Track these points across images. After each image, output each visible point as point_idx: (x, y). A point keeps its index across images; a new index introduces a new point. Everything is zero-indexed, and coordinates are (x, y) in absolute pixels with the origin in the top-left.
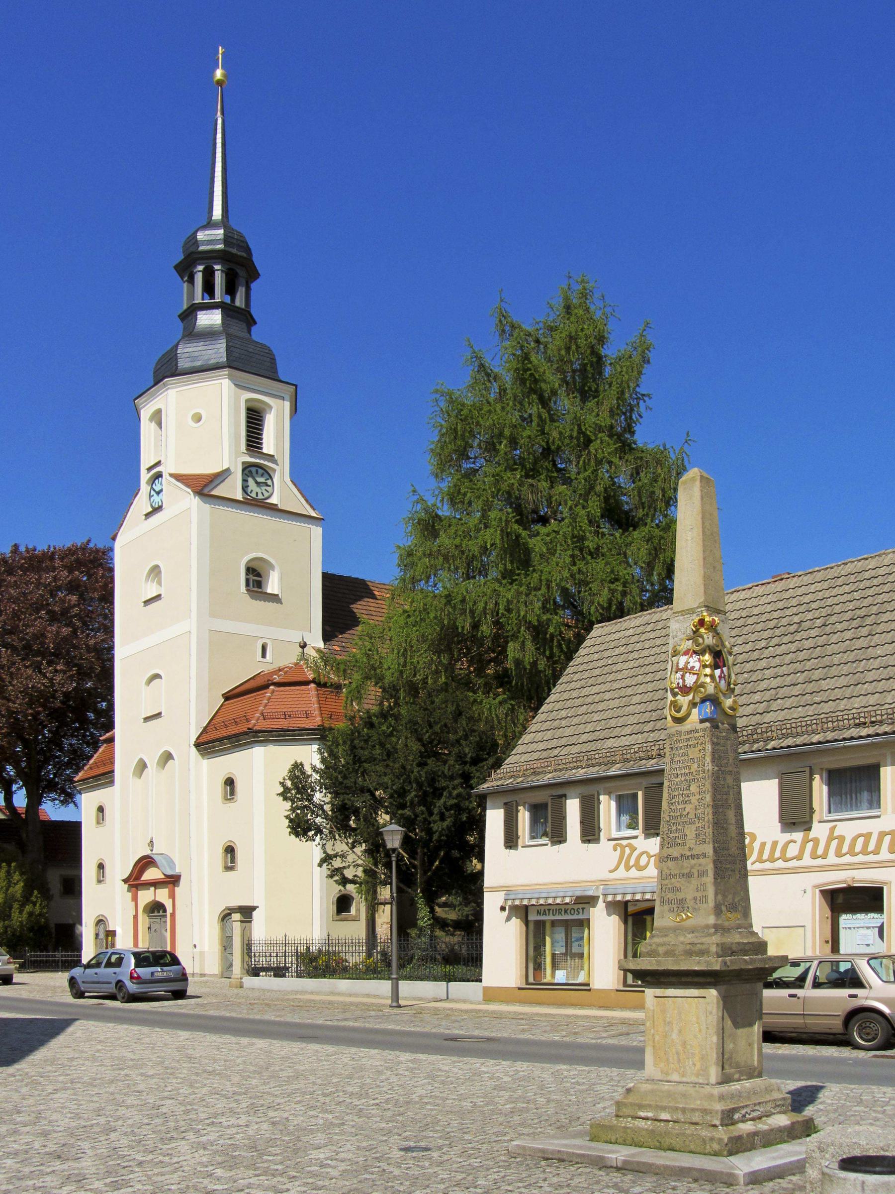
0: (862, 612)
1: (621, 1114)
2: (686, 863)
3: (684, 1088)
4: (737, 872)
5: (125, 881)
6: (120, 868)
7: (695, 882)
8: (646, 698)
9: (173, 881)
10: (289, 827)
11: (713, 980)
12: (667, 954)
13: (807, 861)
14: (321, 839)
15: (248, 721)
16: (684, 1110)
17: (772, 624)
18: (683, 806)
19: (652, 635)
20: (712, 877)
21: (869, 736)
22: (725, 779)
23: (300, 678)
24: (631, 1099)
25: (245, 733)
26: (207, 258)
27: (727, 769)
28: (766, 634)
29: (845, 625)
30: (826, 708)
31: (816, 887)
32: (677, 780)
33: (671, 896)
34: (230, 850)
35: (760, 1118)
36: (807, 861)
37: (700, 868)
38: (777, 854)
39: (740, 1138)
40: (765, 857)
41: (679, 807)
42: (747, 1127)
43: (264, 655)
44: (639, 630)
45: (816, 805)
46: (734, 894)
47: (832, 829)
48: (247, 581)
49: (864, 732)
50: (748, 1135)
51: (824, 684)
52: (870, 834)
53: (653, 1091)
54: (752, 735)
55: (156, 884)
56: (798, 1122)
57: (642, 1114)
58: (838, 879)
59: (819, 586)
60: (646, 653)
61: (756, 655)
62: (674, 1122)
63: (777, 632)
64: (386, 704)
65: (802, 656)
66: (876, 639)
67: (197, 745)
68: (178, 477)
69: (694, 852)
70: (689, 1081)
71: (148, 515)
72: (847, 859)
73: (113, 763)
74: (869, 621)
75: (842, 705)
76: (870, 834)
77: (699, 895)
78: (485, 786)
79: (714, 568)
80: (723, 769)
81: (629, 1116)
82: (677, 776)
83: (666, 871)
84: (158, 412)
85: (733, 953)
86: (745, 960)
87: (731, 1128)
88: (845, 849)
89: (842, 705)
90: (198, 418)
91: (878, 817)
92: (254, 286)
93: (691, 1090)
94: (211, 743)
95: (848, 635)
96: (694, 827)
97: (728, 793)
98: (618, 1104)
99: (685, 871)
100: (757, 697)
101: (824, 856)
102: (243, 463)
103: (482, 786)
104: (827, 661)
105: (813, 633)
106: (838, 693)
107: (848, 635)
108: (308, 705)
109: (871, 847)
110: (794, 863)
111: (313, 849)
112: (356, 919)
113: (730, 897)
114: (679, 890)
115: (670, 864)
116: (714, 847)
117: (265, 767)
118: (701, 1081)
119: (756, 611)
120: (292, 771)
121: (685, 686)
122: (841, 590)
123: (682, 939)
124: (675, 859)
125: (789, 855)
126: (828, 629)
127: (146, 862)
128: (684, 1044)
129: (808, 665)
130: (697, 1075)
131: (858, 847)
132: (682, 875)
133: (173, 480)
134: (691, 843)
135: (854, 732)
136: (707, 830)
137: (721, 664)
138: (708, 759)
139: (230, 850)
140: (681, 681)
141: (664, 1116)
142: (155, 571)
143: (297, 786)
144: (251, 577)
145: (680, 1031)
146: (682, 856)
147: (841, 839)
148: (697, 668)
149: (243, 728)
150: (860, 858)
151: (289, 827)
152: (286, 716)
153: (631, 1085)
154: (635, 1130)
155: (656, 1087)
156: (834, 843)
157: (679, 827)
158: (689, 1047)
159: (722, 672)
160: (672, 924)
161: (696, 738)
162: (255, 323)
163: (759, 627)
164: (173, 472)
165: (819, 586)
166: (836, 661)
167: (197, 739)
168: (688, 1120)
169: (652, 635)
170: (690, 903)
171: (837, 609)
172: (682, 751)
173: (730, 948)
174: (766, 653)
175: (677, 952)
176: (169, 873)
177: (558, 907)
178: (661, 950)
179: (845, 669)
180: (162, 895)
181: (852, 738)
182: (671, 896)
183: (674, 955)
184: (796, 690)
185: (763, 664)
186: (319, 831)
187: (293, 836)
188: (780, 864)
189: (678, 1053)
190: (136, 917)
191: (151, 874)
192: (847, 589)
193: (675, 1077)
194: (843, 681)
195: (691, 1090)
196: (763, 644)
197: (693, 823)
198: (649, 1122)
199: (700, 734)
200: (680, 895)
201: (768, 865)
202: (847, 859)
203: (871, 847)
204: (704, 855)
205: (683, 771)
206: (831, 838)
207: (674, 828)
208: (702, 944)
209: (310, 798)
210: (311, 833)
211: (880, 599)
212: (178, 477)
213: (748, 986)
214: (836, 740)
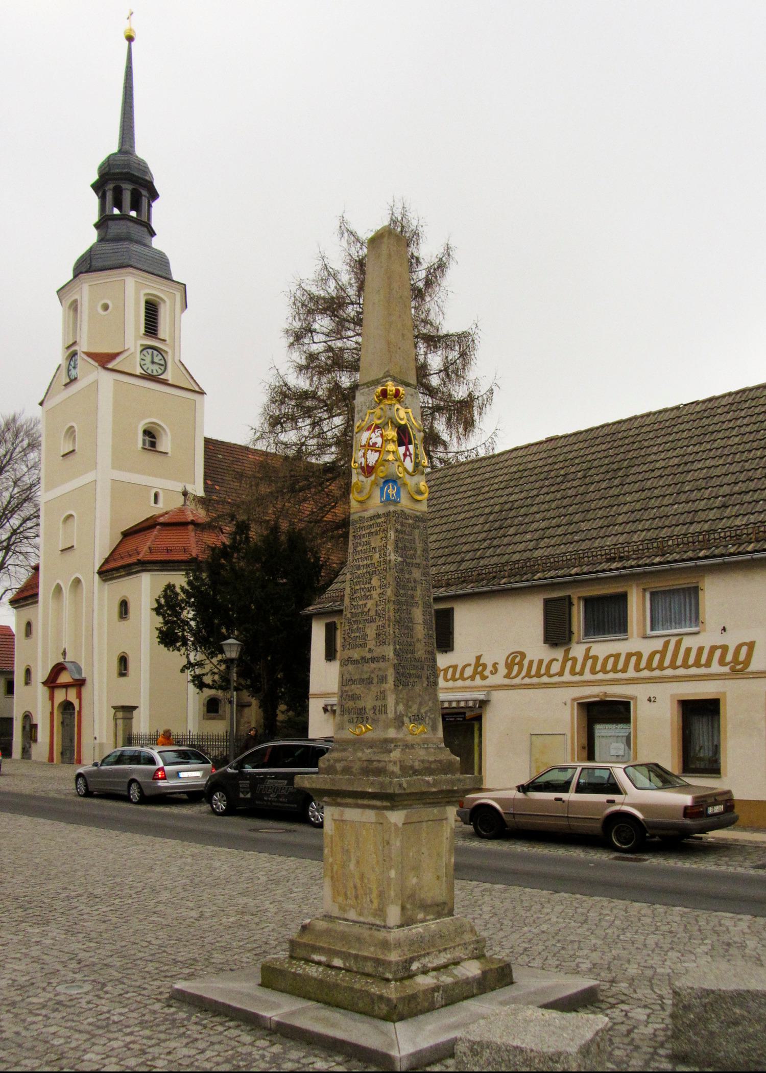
0: (615, 466)
1: (295, 955)
3: (360, 930)
4: (424, 679)
5: (44, 683)
6: (41, 674)
7: (374, 689)
8: (441, 536)
9: (80, 684)
10: (158, 637)
11: (388, 804)
12: (347, 770)
13: (567, 677)
14: (187, 649)
15: (138, 553)
16: (356, 957)
17: (542, 476)
18: (364, 602)
19: (448, 486)
20: (393, 683)
21: (617, 569)
22: (410, 573)
23: (183, 520)
24: (305, 940)
25: (134, 564)
26: (116, 179)
27: (415, 561)
28: (537, 485)
29: (601, 477)
30: (584, 546)
31: (574, 700)
32: (359, 572)
33: (350, 704)
34: (123, 661)
35: (445, 966)
36: (567, 677)
37: (381, 673)
38: (543, 671)
39: (414, 997)
40: (533, 672)
41: (360, 603)
42: (425, 981)
43: (156, 502)
44: (438, 482)
45: (575, 628)
48: (144, 441)
49: (614, 566)
50: (425, 992)
51: (583, 526)
53: (328, 932)
54: (523, 568)
55: (66, 686)
56: (491, 970)
57: (316, 957)
58: (592, 693)
59: (581, 445)
60: (442, 500)
61: (529, 501)
62: (347, 970)
63: (547, 483)
64: (238, 537)
65: (565, 502)
66: (626, 488)
67: (100, 573)
68: (89, 355)
69: (375, 655)
70: (366, 921)
71: (66, 385)
72: (600, 676)
73: (38, 587)
74: (620, 473)
75: (597, 543)
77: (378, 703)
79: (403, 335)
80: (408, 560)
81: (301, 959)
82: (358, 568)
83: (347, 676)
84: (76, 301)
85: (416, 772)
86: (428, 782)
87: (407, 982)
88: (598, 668)
89: (597, 543)
90: (106, 307)
91: (626, 639)
92: (155, 205)
93: (366, 933)
94: (107, 572)
95: (604, 485)
97: (414, 589)
98: (292, 943)
99: (365, 676)
100: (528, 536)
101: (581, 673)
102: (142, 345)
104: (586, 506)
105: (575, 483)
106: (594, 533)
107: (604, 485)
108: (194, 545)
109: (620, 666)
110: (556, 679)
111: (176, 658)
112: (222, 718)
115: (351, 667)
116: (395, 649)
117: (146, 589)
118: (378, 922)
119: (530, 466)
120: (165, 591)
121: (368, 466)
122: (599, 448)
123: (359, 754)
124: (355, 662)
125: (552, 671)
126: (587, 480)
127: (59, 669)
128: (362, 877)
129: (571, 510)
130: (375, 915)
131: (655, 664)
132: (362, 681)
133: (85, 357)
134: (371, 644)
135: (605, 566)
136: (388, 629)
137: (406, 441)
138: (390, 548)
139: (123, 661)
140: (363, 460)
141: (338, 962)
142: (71, 431)
143: (168, 605)
144: (147, 438)
145: (358, 862)
146: (363, 658)
147: (595, 658)
148: (379, 444)
149: (133, 560)
151: (158, 637)
152: (168, 551)
153: (308, 921)
154: (306, 979)
155: (331, 925)
156: (590, 662)
157: (360, 626)
158: (366, 881)
159: (407, 449)
160: (351, 736)
161: (378, 525)
162: (155, 234)
163: (533, 479)
164: (85, 350)
165: (581, 445)
166: (593, 506)
167: (100, 568)
168: (361, 971)
169: (448, 486)
170: (370, 713)
171: (596, 463)
172: (364, 540)
173: (412, 767)
174: (537, 500)
175: (354, 770)
176: (77, 677)
178: (339, 766)
179: (600, 513)
180: (72, 696)
181: (604, 571)
182: (350, 704)
183: (351, 773)
184: (560, 531)
185: (535, 509)
186: (185, 644)
187: (162, 646)
188: (545, 679)
189: (355, 887)
190: (52, 713)
191: (64, 678)
192: (604, 447)
193: (352, 915)
194: (600, 523)
195: (366, 933)
196: (535, 492)
197: (373, 621)
198: (321, 969)
199: (382, 520)
200: (360, 704)
201: (535, 680)
202: (600, 676)
203: (620, 666)
204: (384, 658)
205: (365, 562)
206: (587, 657)
207: (355, 627)
208: (379, 761)
209: (177, 615)
210: (178, 644)
211: (630, 455)
212: (89, 355)
213: (435, 810)
214: (590, 573)
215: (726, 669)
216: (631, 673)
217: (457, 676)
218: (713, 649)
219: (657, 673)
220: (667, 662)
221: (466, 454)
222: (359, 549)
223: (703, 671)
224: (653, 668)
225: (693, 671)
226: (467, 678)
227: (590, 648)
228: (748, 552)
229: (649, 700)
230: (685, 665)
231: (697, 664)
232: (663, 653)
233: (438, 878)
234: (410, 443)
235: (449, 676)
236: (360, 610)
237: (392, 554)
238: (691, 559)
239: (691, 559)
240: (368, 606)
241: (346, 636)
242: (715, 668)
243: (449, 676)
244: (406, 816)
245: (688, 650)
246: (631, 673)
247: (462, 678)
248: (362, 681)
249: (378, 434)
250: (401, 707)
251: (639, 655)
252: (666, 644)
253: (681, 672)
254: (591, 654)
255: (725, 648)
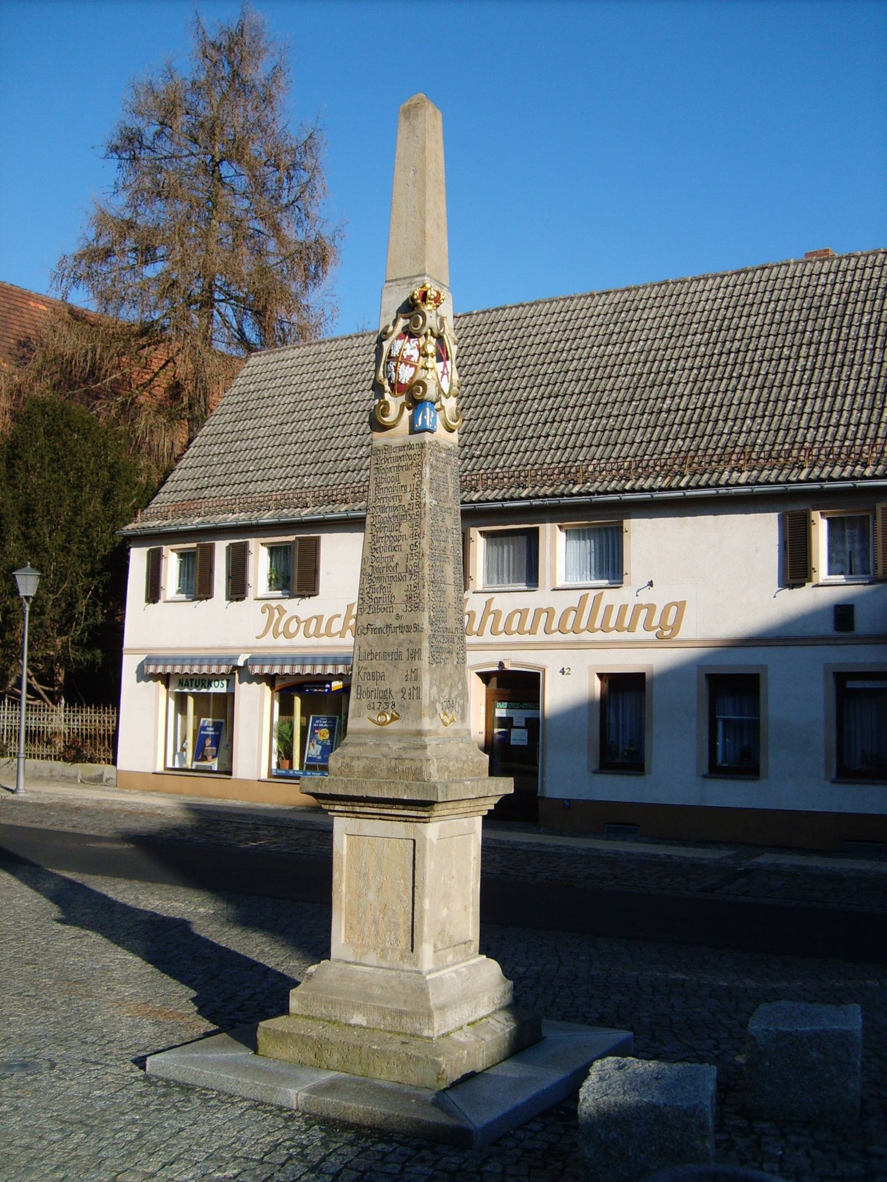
2: (391, 638)
4: (454, 655)
7: (403, 666)
12: (369, 772)
18: (391, 554)
22: (443, 521)
32: (383, 515)
37: (411, 647)
41: (385, 555)
46: (451, 687)
47: (488, 603)
52: (527, 610)
69: (404, 622)
72: (503, 638)
76: (527, 610)
78: (131, 526)
80: (441, 504)
82: (383, 509)
88: (501, 627)
96: (404, 585)
99: (390, 650)
103: (125, 528)
109: (527, 627)
113: (447, 690)
114: (382, 677)
115: (370, 636)
131: (514, 626)
132: (385, 655)
134: (399, 608)
137: (444, 356)
147: (497, 614)
150: (516, 638)
156: (491, 618)
159: (445, 366)
170: (397, 698)
172: (391, 475)
177: (203, 677)
199: (416, 451)
200: (383, 685)
202: (503, 638)
203: (527, 627)
205: (391, 504)
206: (487, 612)
207: (378, 585)
215: (651, 635)
216: (540, 636)
217: (322, 631)
218: (638, 608)
219: (571, 637)
220: (583, 624)
221: (226, 289)
222: (384, 485)
223: (625, 636)
224: (570, 627)
225: (614, 635)
226: (336, 634)
227: (492, 599)
228: (679, 488)
229: (563, 672)
230: (604, 629)
231: (619, 628)
232: (579, 610)
233: (466, 908)
234: (447, 359)
235: (312, 630)
236: (384, 564)
237: (428, 496)
238: (615, 492)
239: (615, 492)
240: (395, 560)
241: (365, 596)
242: (640, 633)
243: (312, 630)
244: (440, 831)
245: (609, 608)
246: (540, 636)
247: (328, 634)
248: (385, 655)
249: (414, 345)
250: (435, 690)
251: (550, 612)
252: (583, 599)
253: (599, 636)
254: (492, 609)
255: (651, 608)
